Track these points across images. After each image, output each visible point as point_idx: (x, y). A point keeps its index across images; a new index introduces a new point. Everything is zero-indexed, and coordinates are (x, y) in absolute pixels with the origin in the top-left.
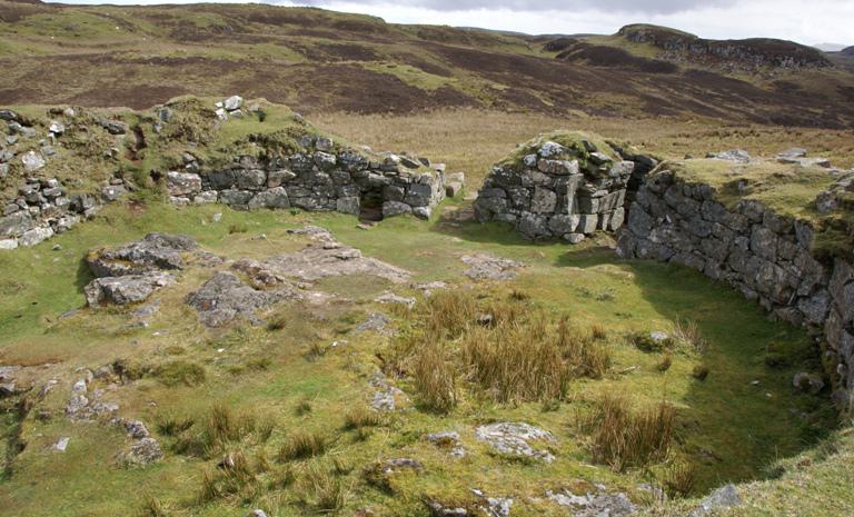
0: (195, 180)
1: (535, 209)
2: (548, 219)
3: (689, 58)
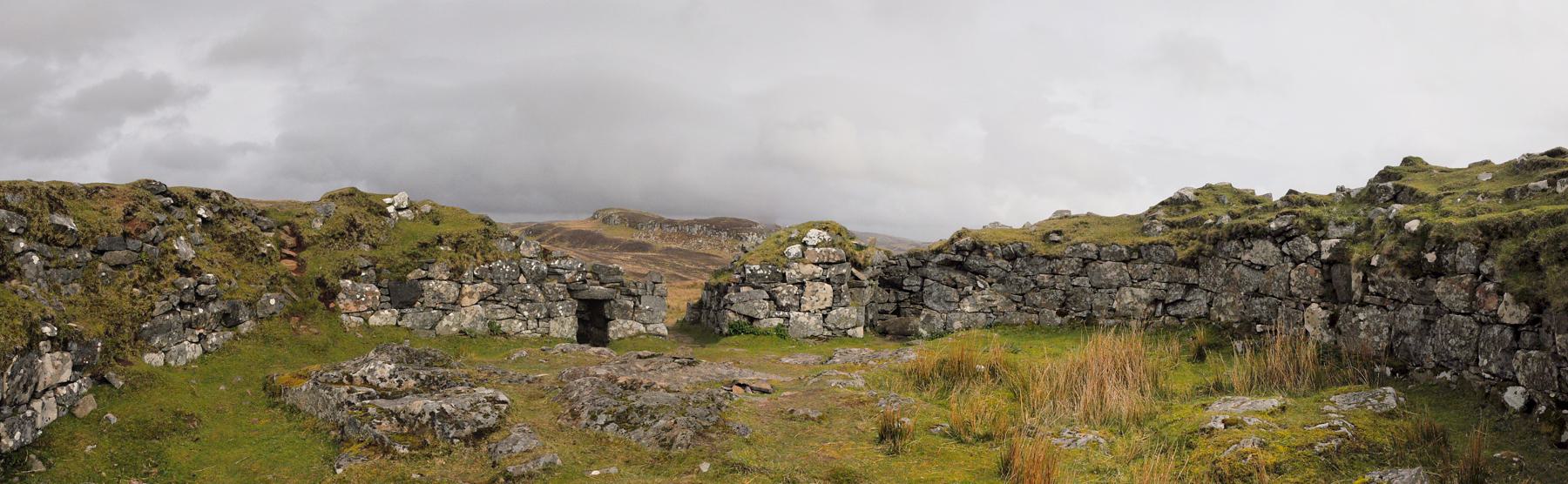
0: (372, 293)
1: (807, 307)
2: (825, 316)
3: (662, 237)
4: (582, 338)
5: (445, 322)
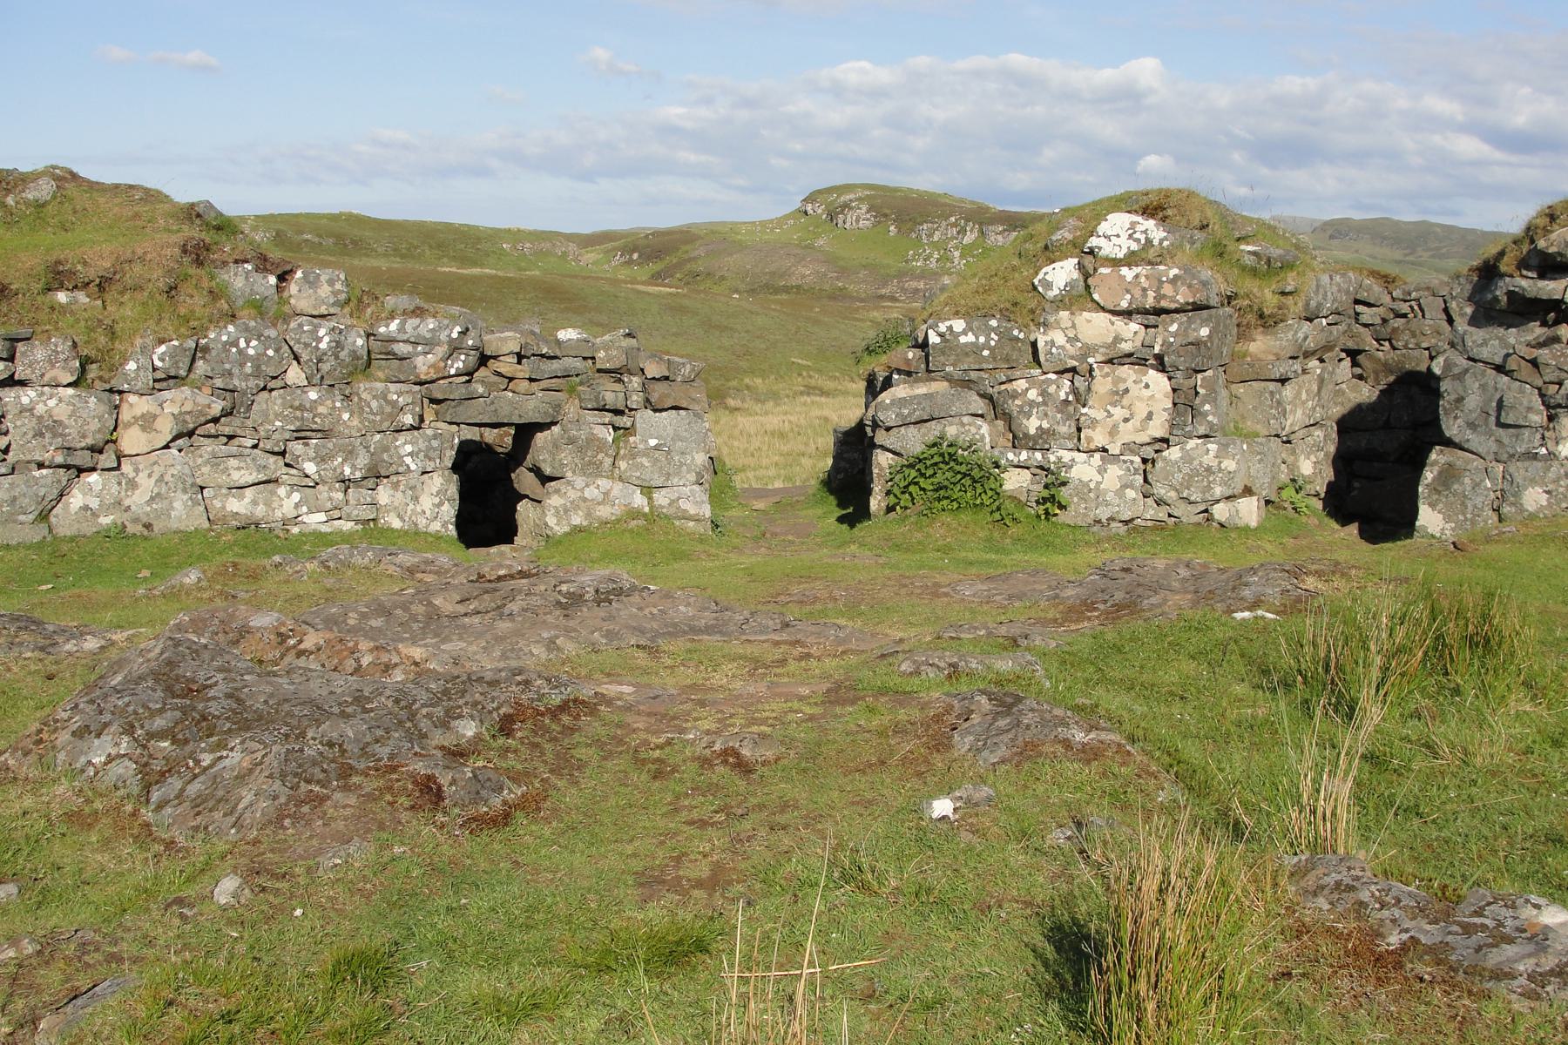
4: (1339, 504)
5: (76, 500)
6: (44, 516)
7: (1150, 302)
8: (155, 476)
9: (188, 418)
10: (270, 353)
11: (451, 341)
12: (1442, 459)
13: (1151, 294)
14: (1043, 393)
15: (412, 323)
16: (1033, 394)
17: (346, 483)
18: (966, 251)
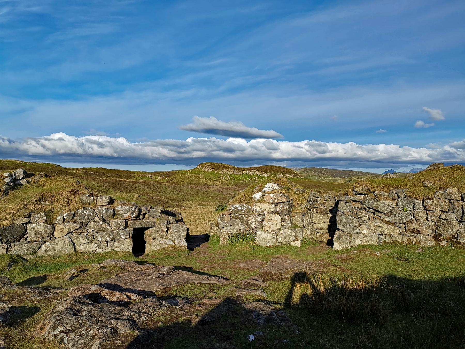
5: (43, 249)
6: (35, 253)
7: (276, 201)
8: (63, 242)
9: (71, 229)
10: (91, 214)
11: (132, 211)
12: (338, 233)
13: (276, 199)
14: (255, 219)
15: (123, 207)
16: (253, 220)
17: (107, 242)
18: (230, 176)
